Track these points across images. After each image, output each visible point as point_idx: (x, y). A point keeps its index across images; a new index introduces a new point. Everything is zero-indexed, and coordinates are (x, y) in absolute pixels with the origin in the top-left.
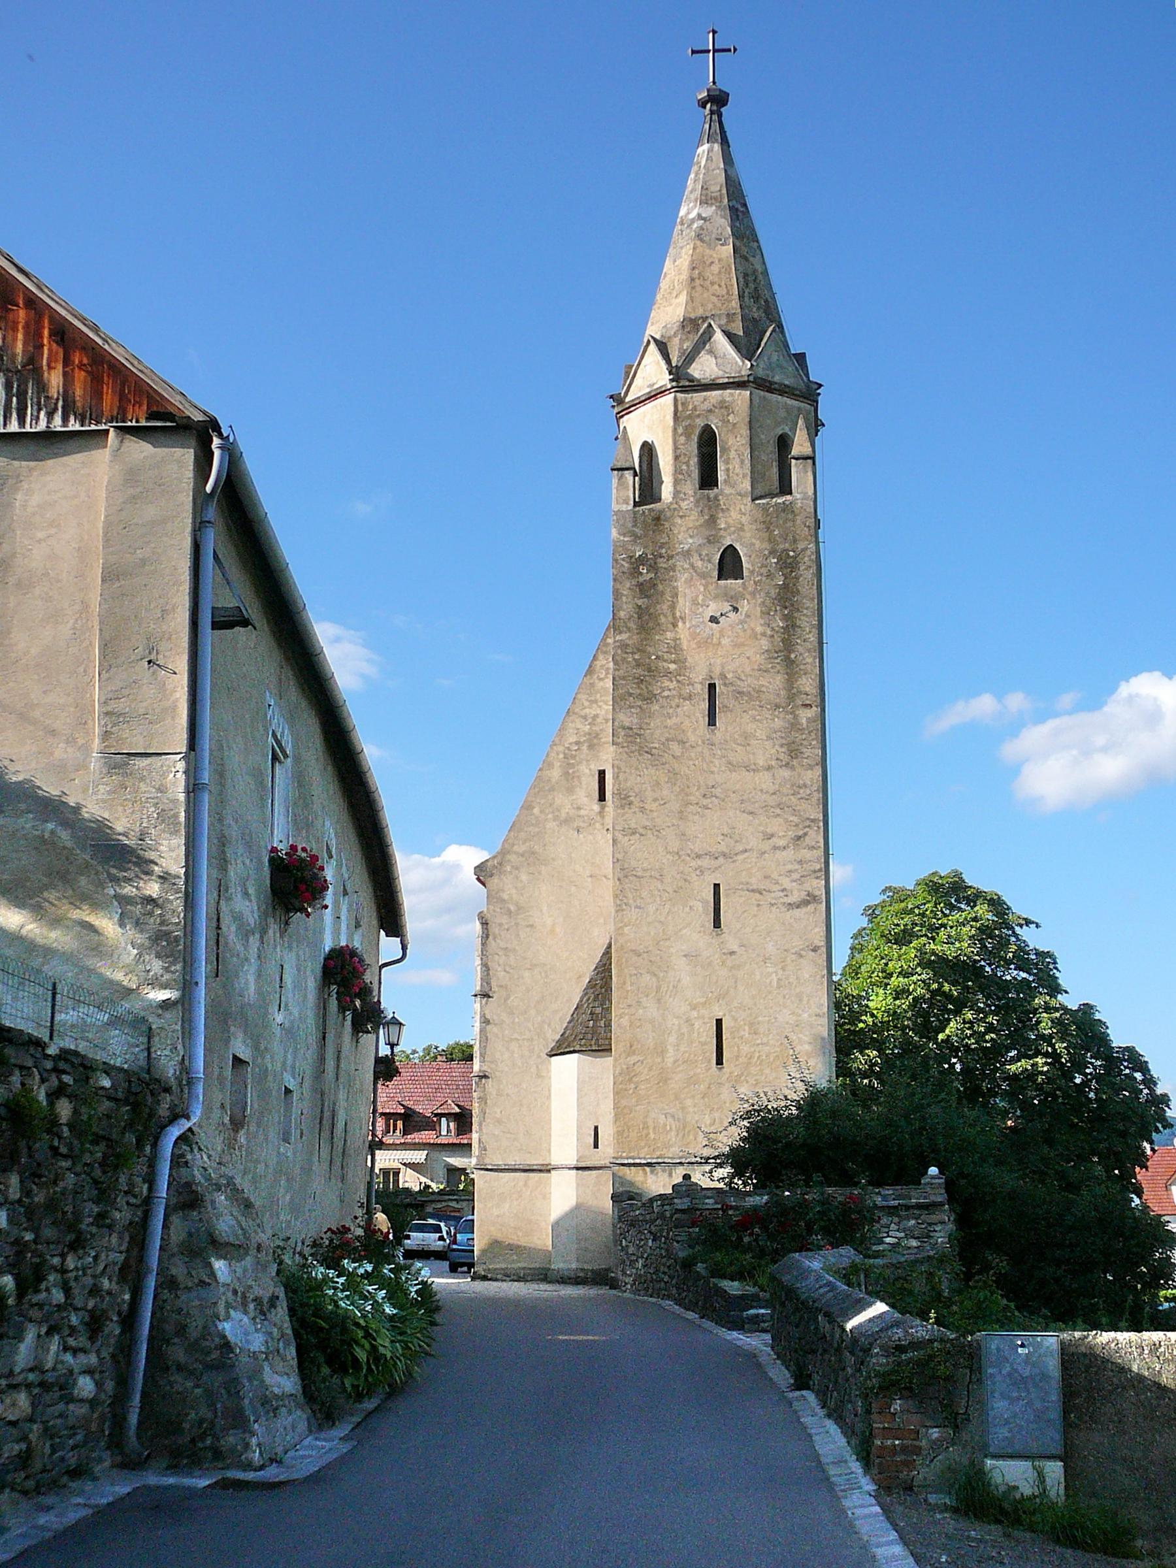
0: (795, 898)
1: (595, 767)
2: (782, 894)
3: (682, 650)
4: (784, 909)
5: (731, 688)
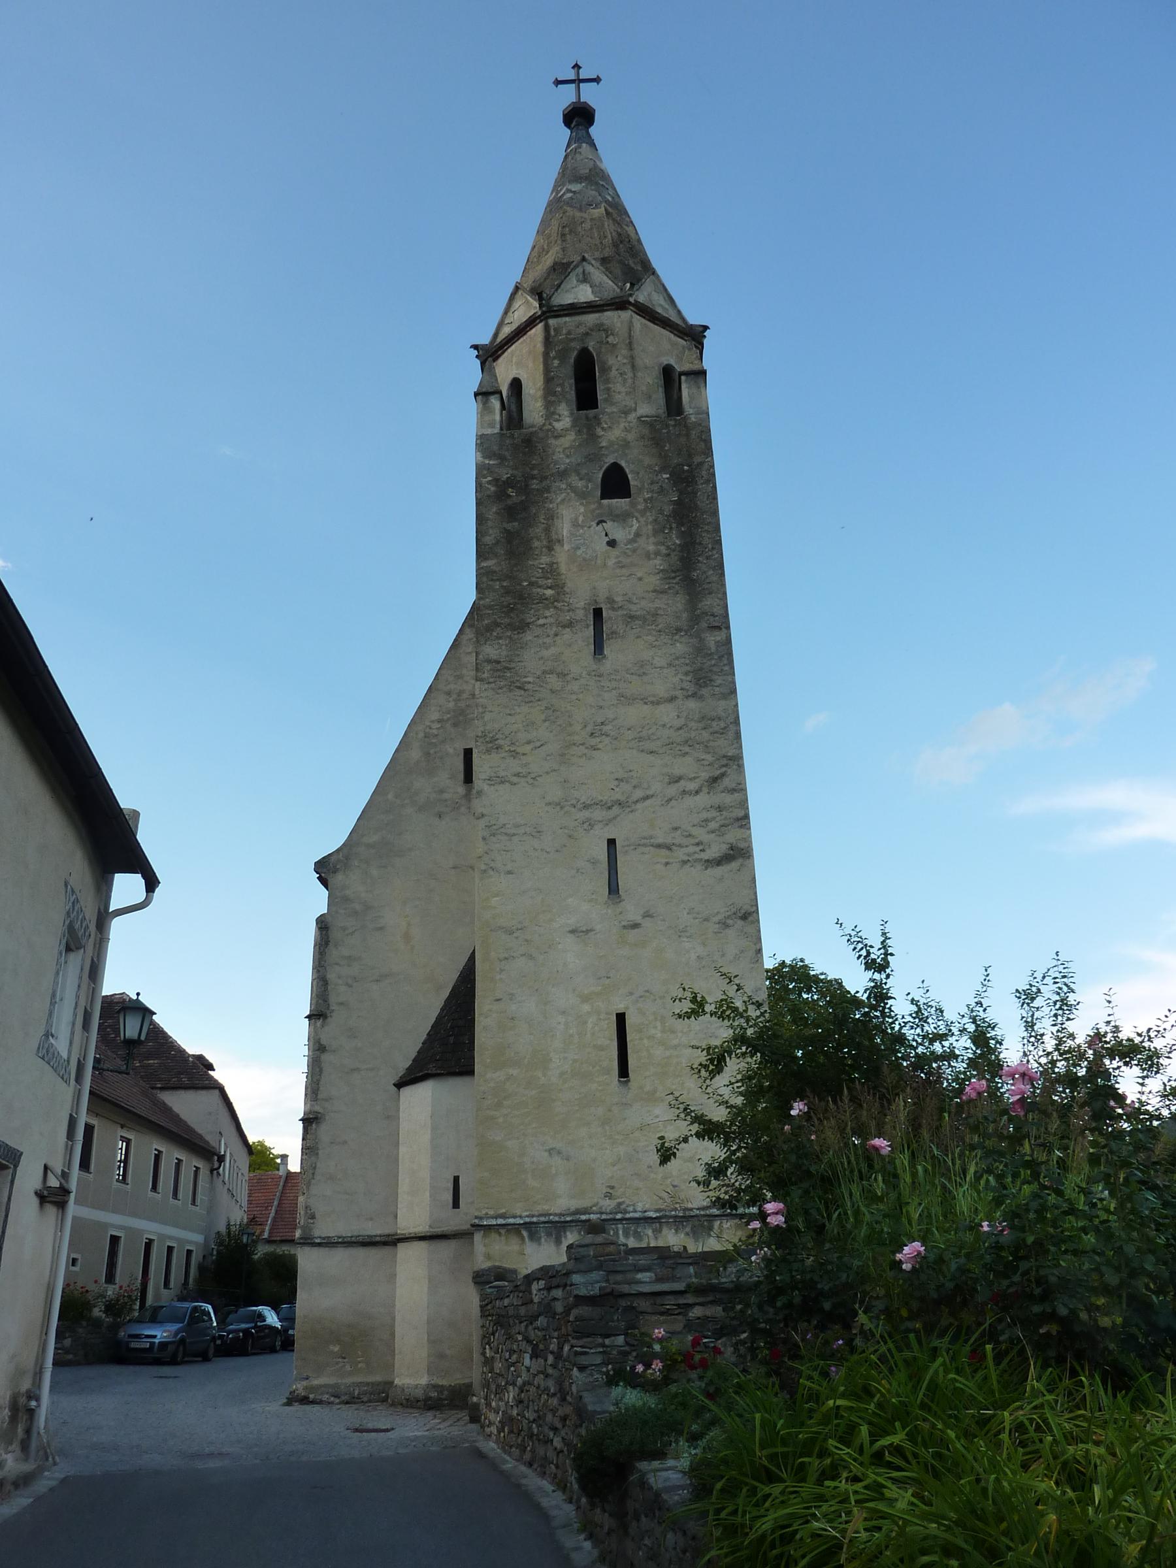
0: (714, 852)
1: (460, 746)
2: (697, 849)
3: (559, 574)
4: (699, 867)
5: (620, 612)
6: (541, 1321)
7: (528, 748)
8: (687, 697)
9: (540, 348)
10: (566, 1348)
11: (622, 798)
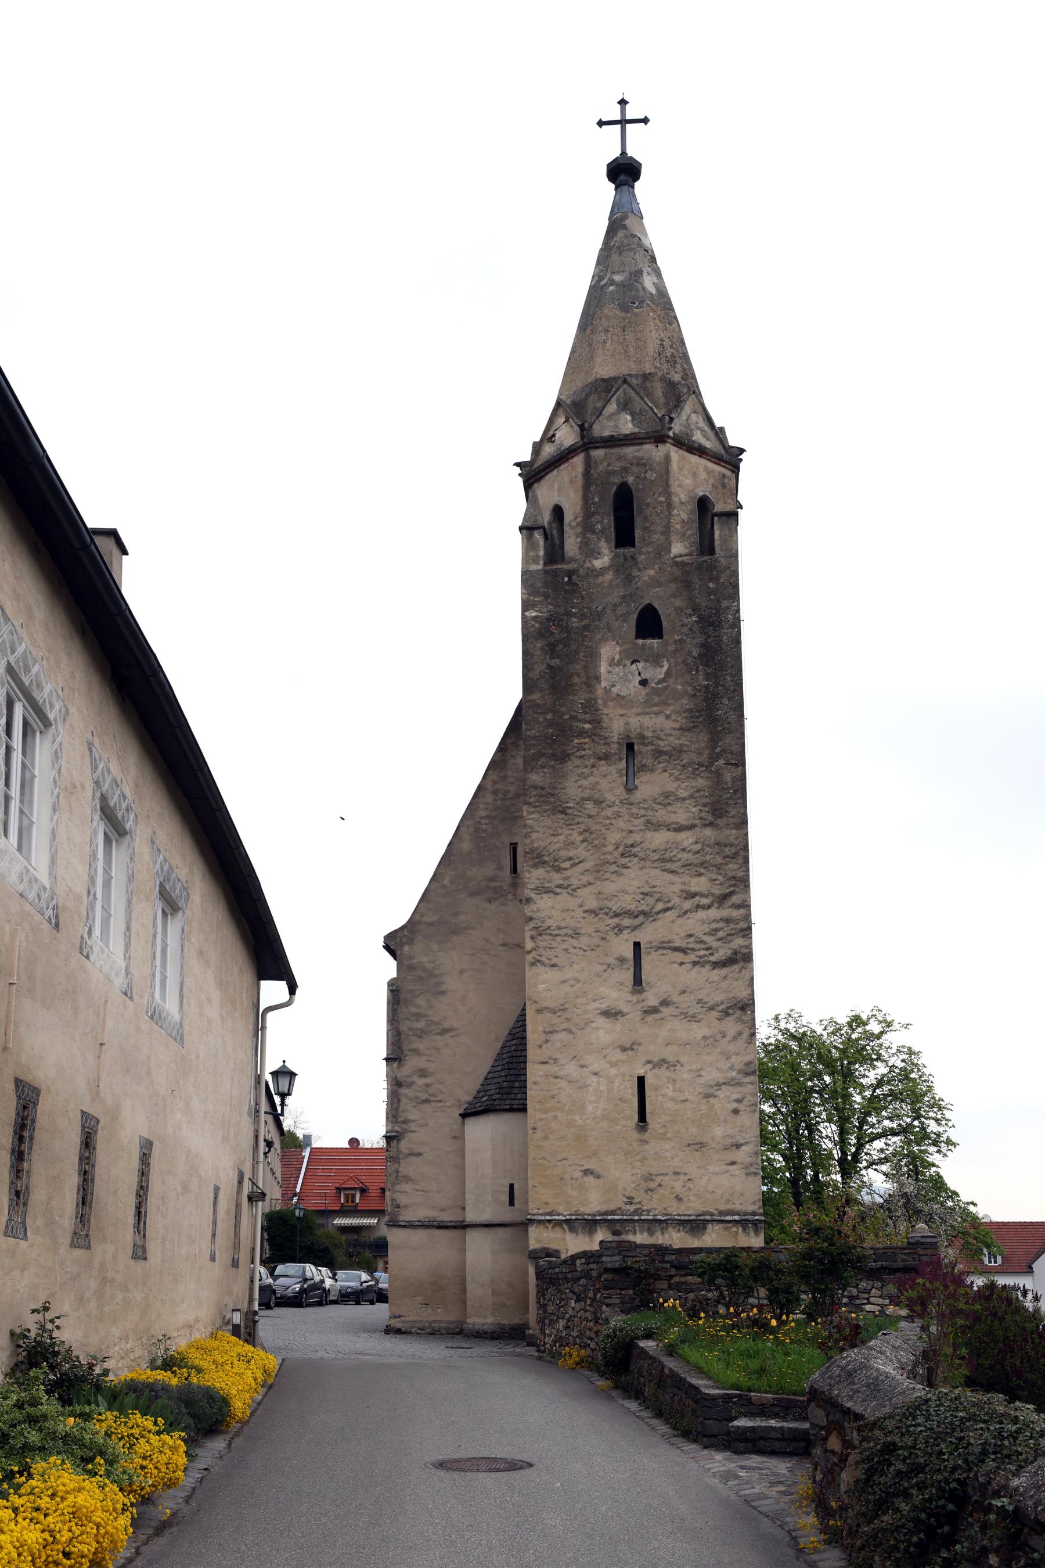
0: (722, 954)
2: (707, 953)
3: (597, 710)
4: (708, 967)
5: (649, 748)
6: (583, 1281)
7: (567, 864)
8: (705, 826)
9: (580, 481)
10: (599, 1295)
11: (647, 909)
